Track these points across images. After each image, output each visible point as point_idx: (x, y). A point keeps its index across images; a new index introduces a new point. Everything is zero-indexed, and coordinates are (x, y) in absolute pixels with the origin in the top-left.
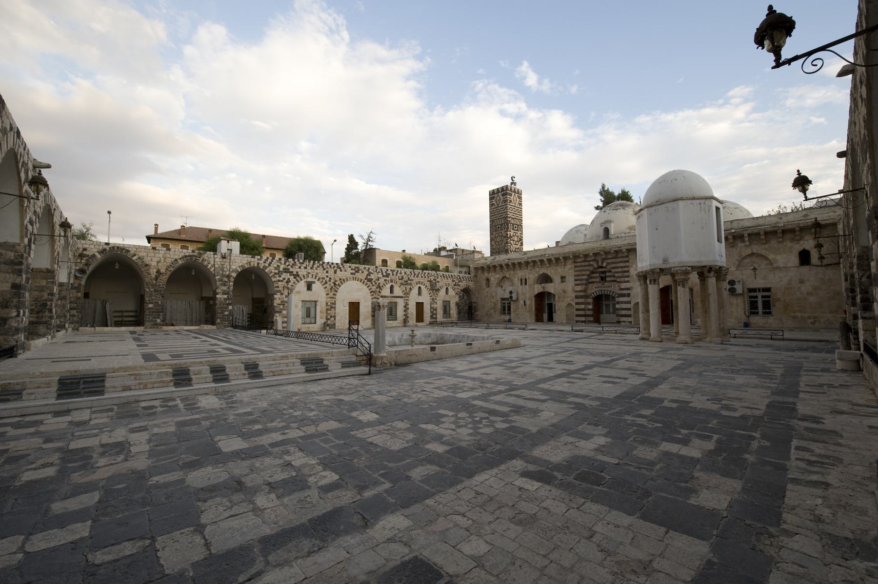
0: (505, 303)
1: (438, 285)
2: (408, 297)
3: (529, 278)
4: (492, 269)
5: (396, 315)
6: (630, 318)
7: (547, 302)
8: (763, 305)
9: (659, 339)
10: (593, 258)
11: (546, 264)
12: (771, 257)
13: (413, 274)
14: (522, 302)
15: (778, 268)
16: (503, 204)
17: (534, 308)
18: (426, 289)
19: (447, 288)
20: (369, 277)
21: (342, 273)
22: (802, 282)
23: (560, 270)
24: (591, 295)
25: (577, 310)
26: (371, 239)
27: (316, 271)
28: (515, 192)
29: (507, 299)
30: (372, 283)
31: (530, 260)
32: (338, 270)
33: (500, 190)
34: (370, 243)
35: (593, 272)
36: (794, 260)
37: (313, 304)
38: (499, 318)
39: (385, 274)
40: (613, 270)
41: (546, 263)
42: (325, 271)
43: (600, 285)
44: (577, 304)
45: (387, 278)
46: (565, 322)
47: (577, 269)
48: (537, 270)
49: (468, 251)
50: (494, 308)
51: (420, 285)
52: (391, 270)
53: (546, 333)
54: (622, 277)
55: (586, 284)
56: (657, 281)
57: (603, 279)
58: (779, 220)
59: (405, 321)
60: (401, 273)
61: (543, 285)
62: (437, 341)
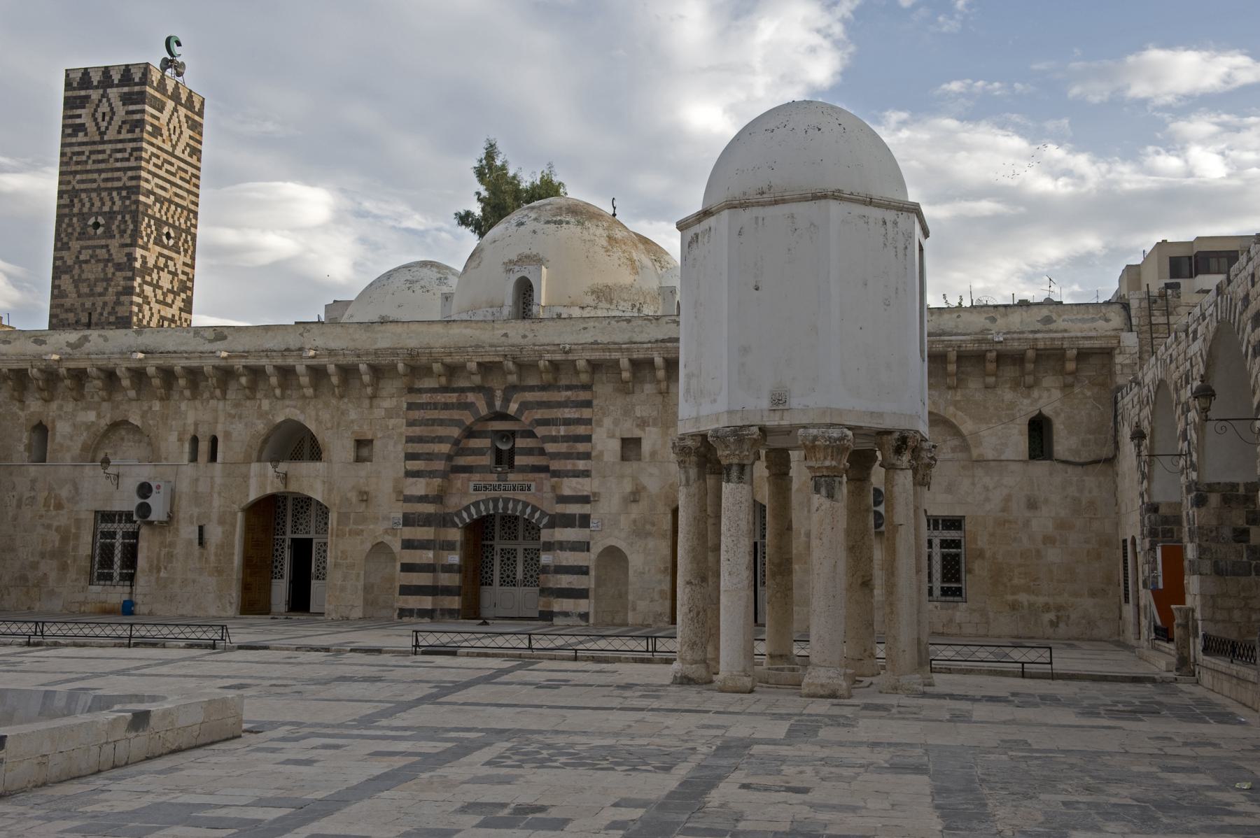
0: (112, 535)
3: (227, 435)
4: (68, 382)
6: (583, 602)
7: (289, 535)
8: (944, 567)
9: (747, 682)
10: (477, 380)
11: (301, 387)
12: (967, 427)
14: (188, 532)
15: (981, 461)
16: (124, 135)
17: (237, 560)
22: (1032, 505)
24: (458, 514)
25: (407, 568)
28: (175, 97)
29: (128, 516)
31: (238, 364)
33: (116, 78)
35: (470, 433)
36: (1019, 441)
38: (81, 597)
40: (540, 431)
41: (305, 380)
43: (492, 479)
44: (408, 544)
46: (357, 613)
47: (416, 414)
48: (266, 404)
50: (59, 554)
53: (316, 667)
54: (568, 456)
55: (445, 475)
56: (747, 470)
57: (504, 459)
58: (988, 324)
61: (283, 467)
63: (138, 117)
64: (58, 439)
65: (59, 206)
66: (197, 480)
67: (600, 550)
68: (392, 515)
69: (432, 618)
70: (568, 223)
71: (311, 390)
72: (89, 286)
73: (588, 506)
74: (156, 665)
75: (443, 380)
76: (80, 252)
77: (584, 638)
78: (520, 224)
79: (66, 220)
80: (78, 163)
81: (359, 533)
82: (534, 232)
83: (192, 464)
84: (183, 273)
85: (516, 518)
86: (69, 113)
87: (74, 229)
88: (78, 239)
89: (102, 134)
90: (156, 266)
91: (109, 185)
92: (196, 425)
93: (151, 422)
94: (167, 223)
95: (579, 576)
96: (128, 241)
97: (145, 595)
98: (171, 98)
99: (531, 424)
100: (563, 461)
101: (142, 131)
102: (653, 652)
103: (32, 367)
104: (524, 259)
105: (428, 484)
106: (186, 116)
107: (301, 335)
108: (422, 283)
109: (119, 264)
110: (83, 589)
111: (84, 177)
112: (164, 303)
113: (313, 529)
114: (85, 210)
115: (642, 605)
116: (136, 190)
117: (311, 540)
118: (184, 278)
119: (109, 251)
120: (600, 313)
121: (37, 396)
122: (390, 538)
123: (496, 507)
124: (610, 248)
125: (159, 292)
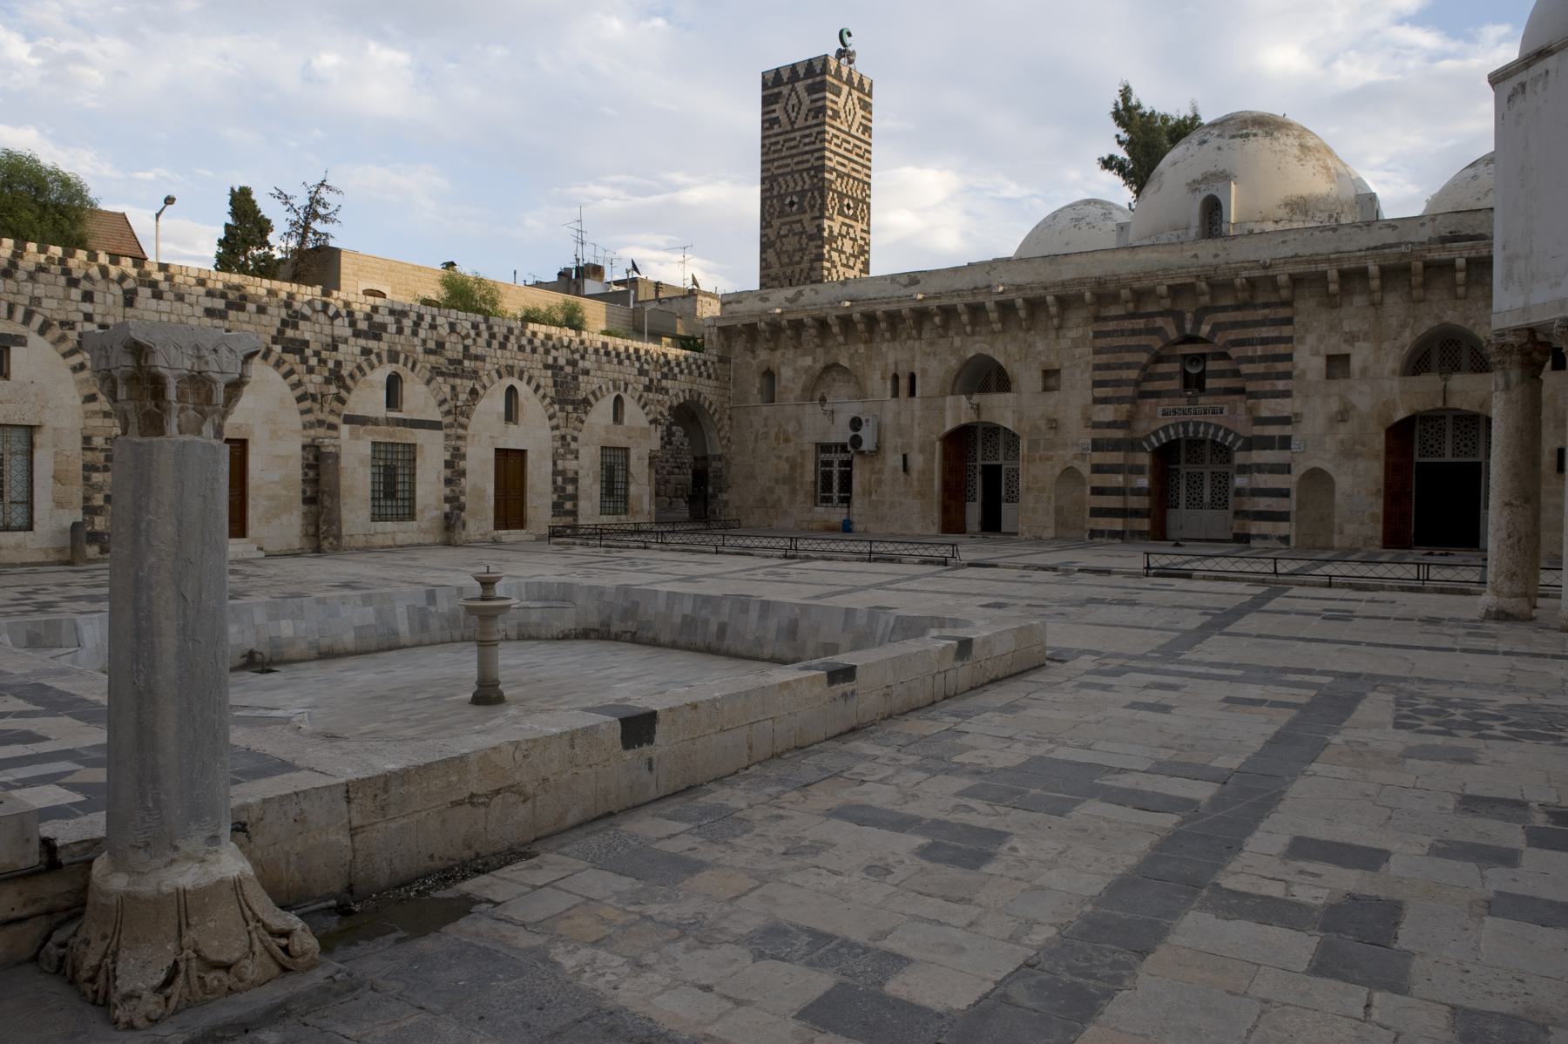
0: (829, 463)
1: (586, 386)
2: (464, 427)
3: (924, 371)
4: (789, 332)
5: (412, 499)
7: (980, 462)
10: (1167, 303)
13: (485, 335)
14: (894, 460)
16: (811, 122)
18: (535, 399)
19: (618, 400)
20: (290, 333)
21: (164, 305)
23: (1040, 346)
24: (1147, 439)
25: (1097, 491)
26: (321, 211)
27: (28, 288)
28: (849, 82)
29: (843, 448)
30: (304, 361)
32: (145, 292)
33: (801, 72)
34: (317, 225)
35: (1158, 359)
37: (17, 442)
39: (363, 325)
40: (1234, 352)
41: (994, 316)
42: (76, 294)
43: (1182, 403)
44: (1097, 469)
45: (372, 344)
46: (1050, 533)
47: (1102, 342)
48: (957, 341)
49: (678, 289)
51: (514, 381)
52: (392, 312)
54: (1265, 376)
55: (1132, 400)
57: (1194, 383)
59: (451, 526)
60: (433, 327)
61: (976, 398)
62: (607, 624)
63: (820, 104)
64: (783, 382)
65: (762, 191)
66: (899, 413)
67: (1302, 472)
68: (1081, 442)
69: (1122, 539)
70: (1255, 135)
71: (1000, 325)
72: (789, 257)
73: (1290, 427)
74: (905, 580)
75: (1131, 306)
76: (780, 229)
77: (1189, 558)
78: (1203, 142)
79: (769, 202)
80: (775, 152)
81: (1049, 459)
82: (1219, 148)
83: (894, 399)
84: (862, 238)
85: (1203, 441)
86: (767, 109)
87: (775, 209)
88: (778, 217)
89: (792, 123)
90: (840, 234)
91: (800, 167)
92: (896, 364)
93: (857, 363)
94: (847, 196)
95: (1280, 499)
96: (817, 214)
97: (860, 515)
98: (846, 83)
99: (1224, 345)
100: (1260, 383)
101: (824, 116)
102: (1423, 580)
103: (760, 321)
104: (1209, 178)
105: (1116, 410)
106: (859, 98)
107: (988, 273)
108: (1088, 220)
109: (811, 235)
110: (810, 510)
111: (780, 163)
112: (846, 266)
113: (1001, 456)
114: (783, 191)
115: (1350, 529)
116: (822, 168)
117: (1000, 466)
118: (862, 243)
119: (802, 224)
120: (1295, 226)
121: (765, 346)
122: (1079, 463)
123: (1186, 431)
124: (1303, 156)
125: (843, 256)
